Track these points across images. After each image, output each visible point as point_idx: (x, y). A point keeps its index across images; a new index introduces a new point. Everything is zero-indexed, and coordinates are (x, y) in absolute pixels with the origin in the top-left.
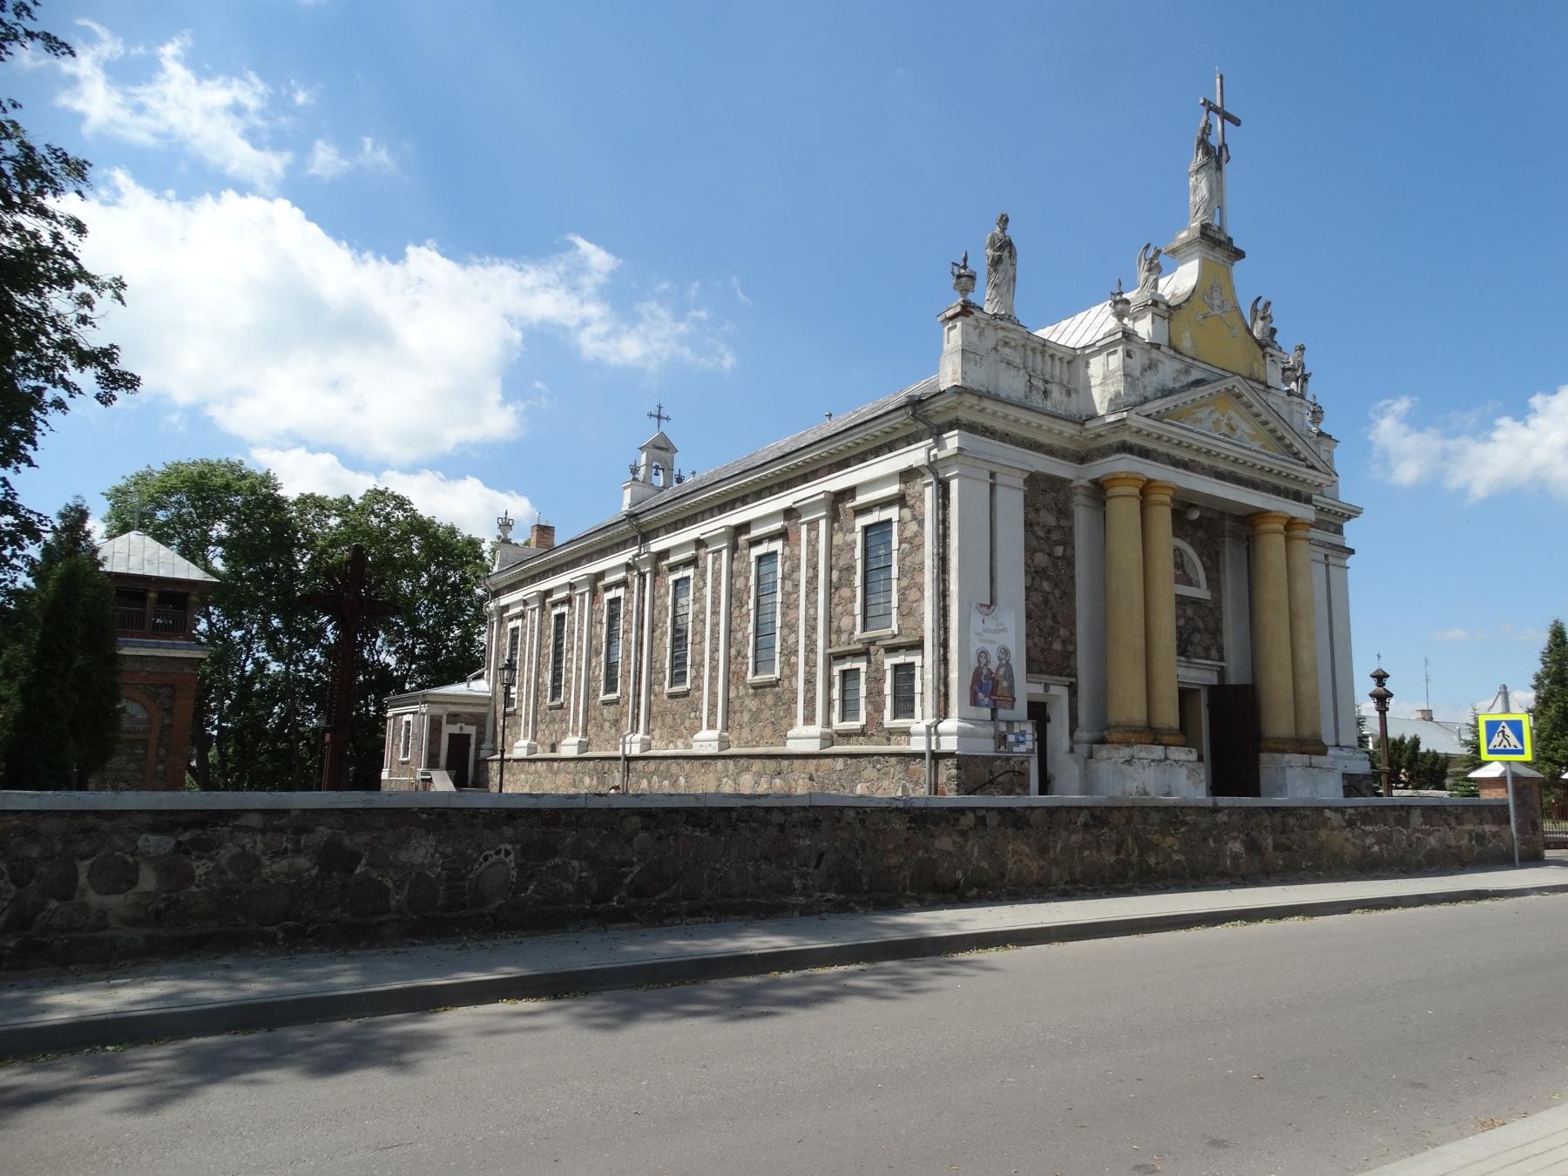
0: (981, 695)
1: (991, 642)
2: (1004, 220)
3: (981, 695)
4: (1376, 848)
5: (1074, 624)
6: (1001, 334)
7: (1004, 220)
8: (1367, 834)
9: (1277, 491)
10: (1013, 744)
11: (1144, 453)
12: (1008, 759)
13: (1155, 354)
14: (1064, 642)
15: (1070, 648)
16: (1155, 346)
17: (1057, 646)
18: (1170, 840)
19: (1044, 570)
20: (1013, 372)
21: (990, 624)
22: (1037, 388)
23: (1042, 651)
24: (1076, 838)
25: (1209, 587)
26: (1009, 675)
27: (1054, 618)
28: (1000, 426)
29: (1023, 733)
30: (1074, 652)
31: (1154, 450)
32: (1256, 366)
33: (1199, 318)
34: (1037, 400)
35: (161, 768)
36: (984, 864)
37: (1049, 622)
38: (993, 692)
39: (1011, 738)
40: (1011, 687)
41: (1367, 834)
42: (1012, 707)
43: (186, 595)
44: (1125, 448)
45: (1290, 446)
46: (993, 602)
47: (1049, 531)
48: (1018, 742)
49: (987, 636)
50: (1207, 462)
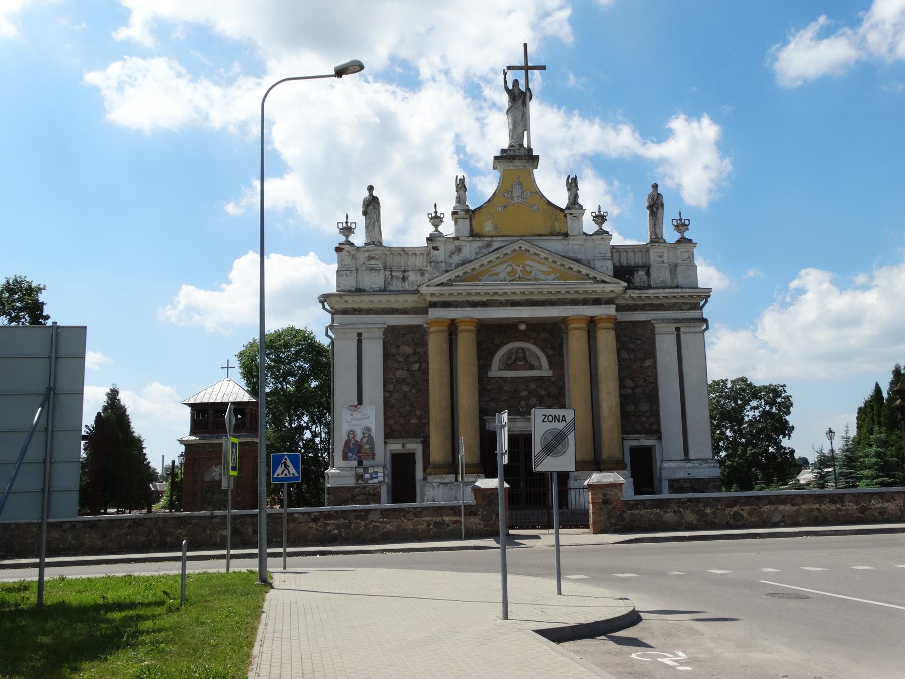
0: (350, 454)
1: (358, 425)
2: (371, 188)
3: (350, 454)
4: (336, 531)
5: (428, 407)
6: (367, 254)
7: (371, 188)
8: (329, 525)
9: (575, 302)
10: (368, 479)
11: (446, 305)
12: (364, 487)
13: (457, 243)
14: (420, 418)
15: (424, 421)
16: (456, 238)
17: (414, 421)
18: (180, 531)
19: (404, 380)
20: (375, 273)
21: (357, 415)
22: (397, 277)
23: (402, 425)
24: (125, 531)
25: (550, 368)
26: (371, 440)
27: (412, 405)
28: (364, 306)
29: (376, 473)
30: (428, 423)
31: (455, 301)
32: (557, 225)
33: (500, 209)
34: (397, 285)
35: (239, 499)
36: (73, 542)
37: (408, 408)
38: (359, 452)
39: (367, 476)
40: (372, 448)
41: (329, 525)
42: (373, 459)
43: (245, 409)
44: (434, 305)
45: (579, 272)
46: (360, 402)
47: (408, 357)
48: (372, 478)
49: (356, 422)
50: (503, 298)
